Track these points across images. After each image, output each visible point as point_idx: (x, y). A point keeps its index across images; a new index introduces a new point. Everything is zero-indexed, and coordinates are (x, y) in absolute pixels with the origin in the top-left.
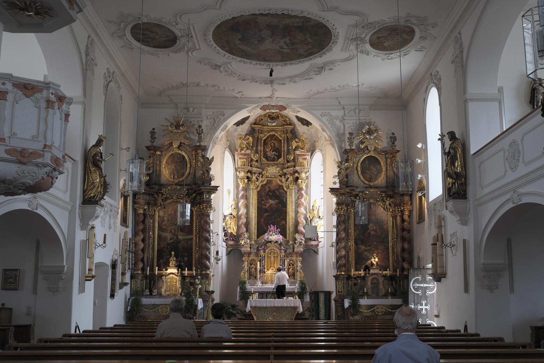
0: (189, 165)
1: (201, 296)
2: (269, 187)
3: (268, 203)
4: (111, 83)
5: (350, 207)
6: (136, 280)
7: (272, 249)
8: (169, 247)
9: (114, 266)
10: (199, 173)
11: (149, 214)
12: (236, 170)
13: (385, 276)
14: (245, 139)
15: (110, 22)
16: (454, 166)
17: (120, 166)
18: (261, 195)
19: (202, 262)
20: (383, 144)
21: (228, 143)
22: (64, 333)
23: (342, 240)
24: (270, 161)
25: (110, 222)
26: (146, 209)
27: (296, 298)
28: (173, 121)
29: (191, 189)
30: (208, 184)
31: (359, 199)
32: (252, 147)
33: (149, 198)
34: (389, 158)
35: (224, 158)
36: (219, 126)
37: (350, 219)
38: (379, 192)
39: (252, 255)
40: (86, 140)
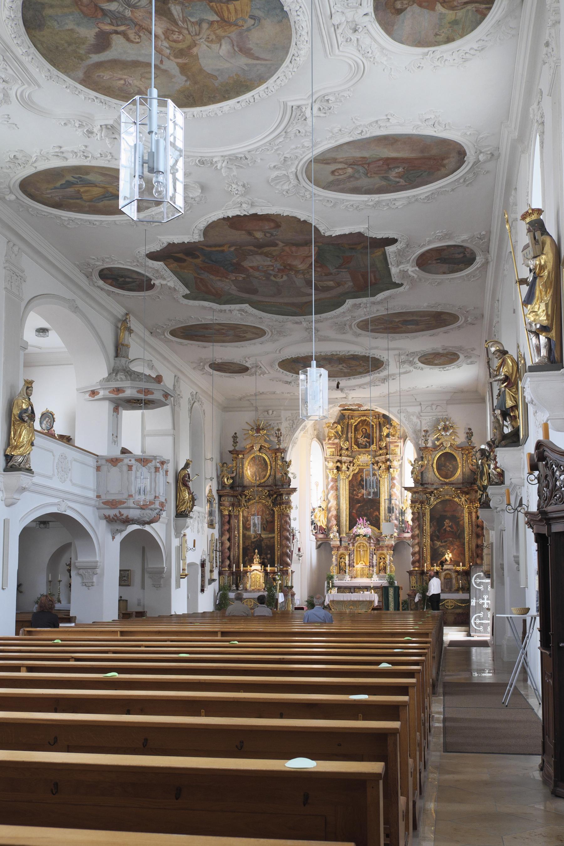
0: (269, 467)
1: (282, 590)
2: (361, 476)
3: (360, 493)
4: (195, 404)
5: (426, 504)
8: (253, 545)
9: (203, 565)
10: (279, 476)
13: (457, 572)
14: (333, 428)
15: (191, 363)
16: (482, 480)
17: (205, 475)
18: (352, 485)
20: (461, 439)
21: (316, 433)
22: (521, 215)
23: (415, 536)
25: (198, 526)
27: (371, 593)
30: (287, 486)
31: (434, 496)
33: (234, 499)
34: (466, 454)
35: (310, 450)
36: (297, 427)
37: (425, 515)
38: (453, 489)
39: (341, 549)
40: (176, 464)
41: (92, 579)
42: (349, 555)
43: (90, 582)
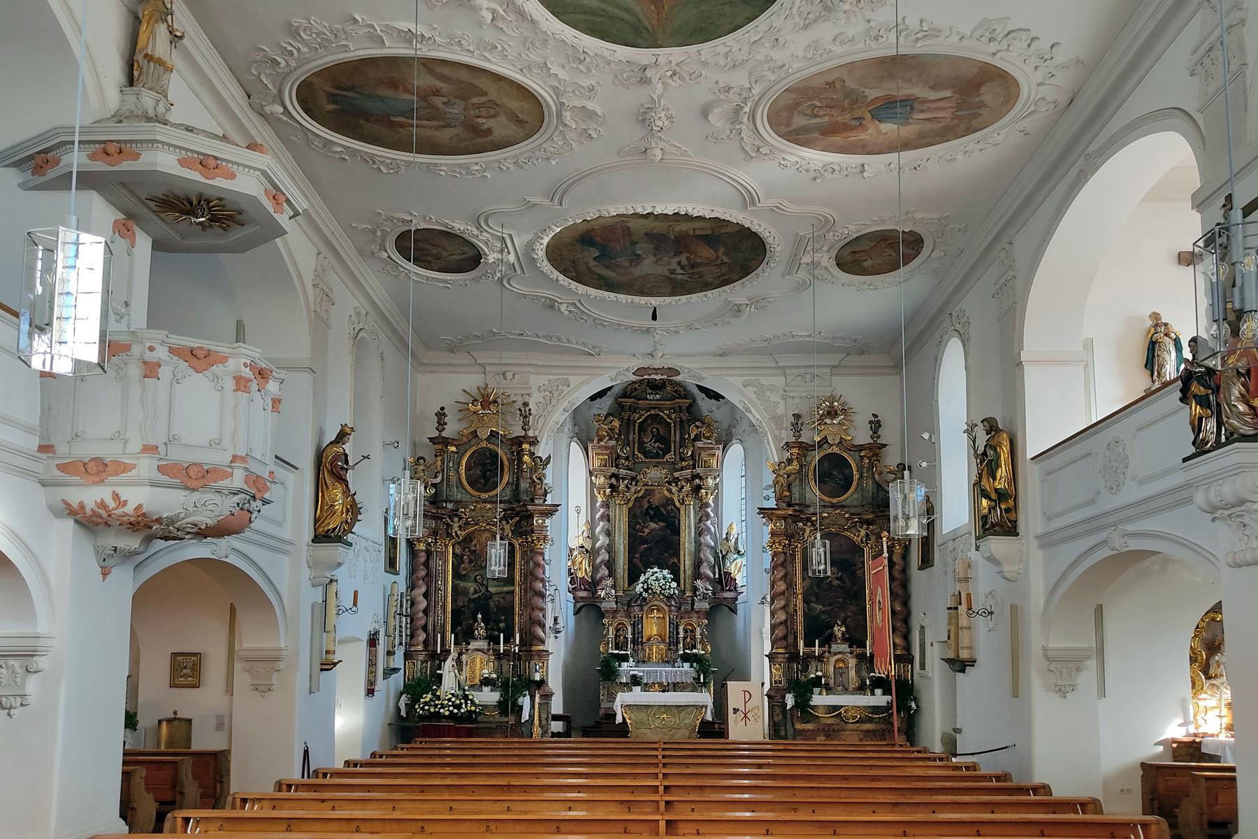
2: (649, 502)
3: (647, 527)
6: (413, 661)
7: (653, 606)
9: (373, 642)
11: (437, 551)
12: (591, 473)
19: (532, 631)
21: (577, 430)
24: (652, 458)
26: (432, 542)
28: (474, 392)
29: (510, 509)
30: (541, 502)
32: (619, 435)
39: (619, 615)
40: (321, 434)
41: (23, 686)
42: (633, 625)
43: (15, 696)
